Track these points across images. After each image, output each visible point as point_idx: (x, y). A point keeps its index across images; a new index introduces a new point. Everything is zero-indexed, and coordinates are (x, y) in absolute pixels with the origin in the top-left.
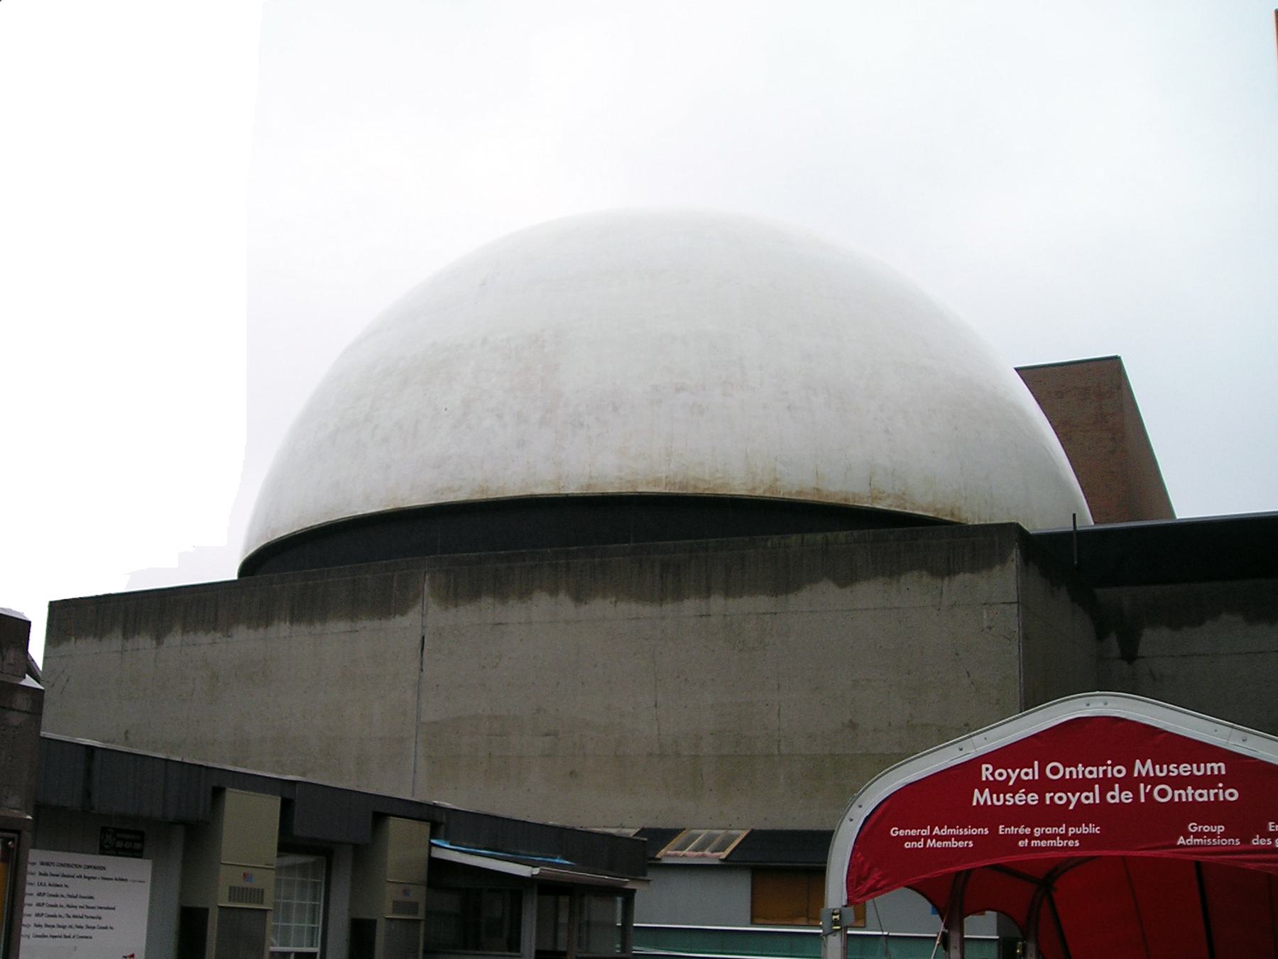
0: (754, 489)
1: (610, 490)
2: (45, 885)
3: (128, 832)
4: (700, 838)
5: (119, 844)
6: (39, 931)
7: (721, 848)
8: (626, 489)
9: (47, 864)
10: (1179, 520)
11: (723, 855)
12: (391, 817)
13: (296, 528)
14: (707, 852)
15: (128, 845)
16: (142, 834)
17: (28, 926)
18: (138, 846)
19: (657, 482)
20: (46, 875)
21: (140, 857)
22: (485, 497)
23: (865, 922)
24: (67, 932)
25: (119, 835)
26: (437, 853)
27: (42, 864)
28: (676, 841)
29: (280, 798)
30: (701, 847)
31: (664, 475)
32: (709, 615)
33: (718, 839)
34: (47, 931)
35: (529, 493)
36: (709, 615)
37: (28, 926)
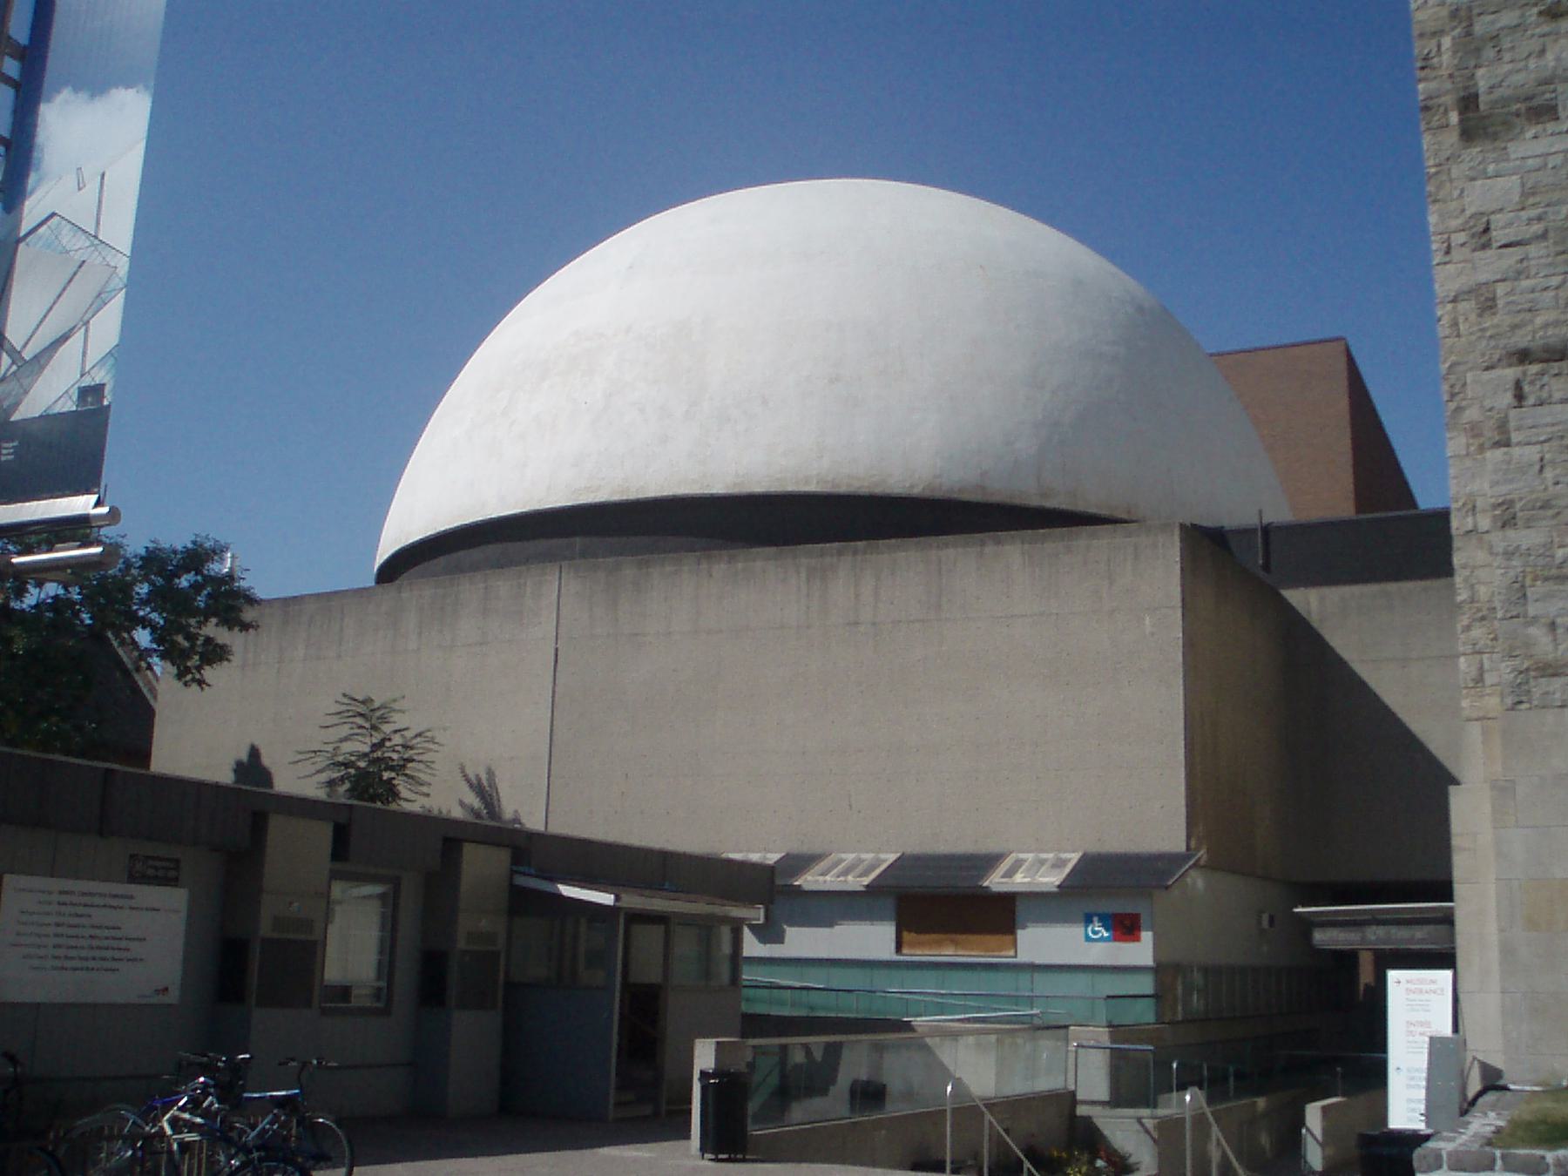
0: (912, 486)
1: (758, 488)
2: (64, 914)
3: (160, 859)
4: (843, 864)
5: (150, 872)
6: (58, 963)
7: (865, 873)
8: (775, 488)
9: (66, 893)
10: (1423, 510)
11: (866, 881)
12: (467, 844)
13: (430, 532)
14: (850, 878)
15: (160, 873)
16: (177, 861)
17: (1460, 589)
18: (172, 874)
19: (807, 481)
20: (64, 904)
21: (176, 886)
22: (625, 498)
23: (1016, 952)
24: (91, 964)
25: (151, 862)
26: (521, 881)
27: (61, 893)
28: (823, 865)
29: (332, 824)
30: (846, 872)
31: (815, 472)
32: (858, 623)
33: (866, 863)
34: (69, 964)
35: (671, 494)
36: (858, 623)
37: (1460, 589)
